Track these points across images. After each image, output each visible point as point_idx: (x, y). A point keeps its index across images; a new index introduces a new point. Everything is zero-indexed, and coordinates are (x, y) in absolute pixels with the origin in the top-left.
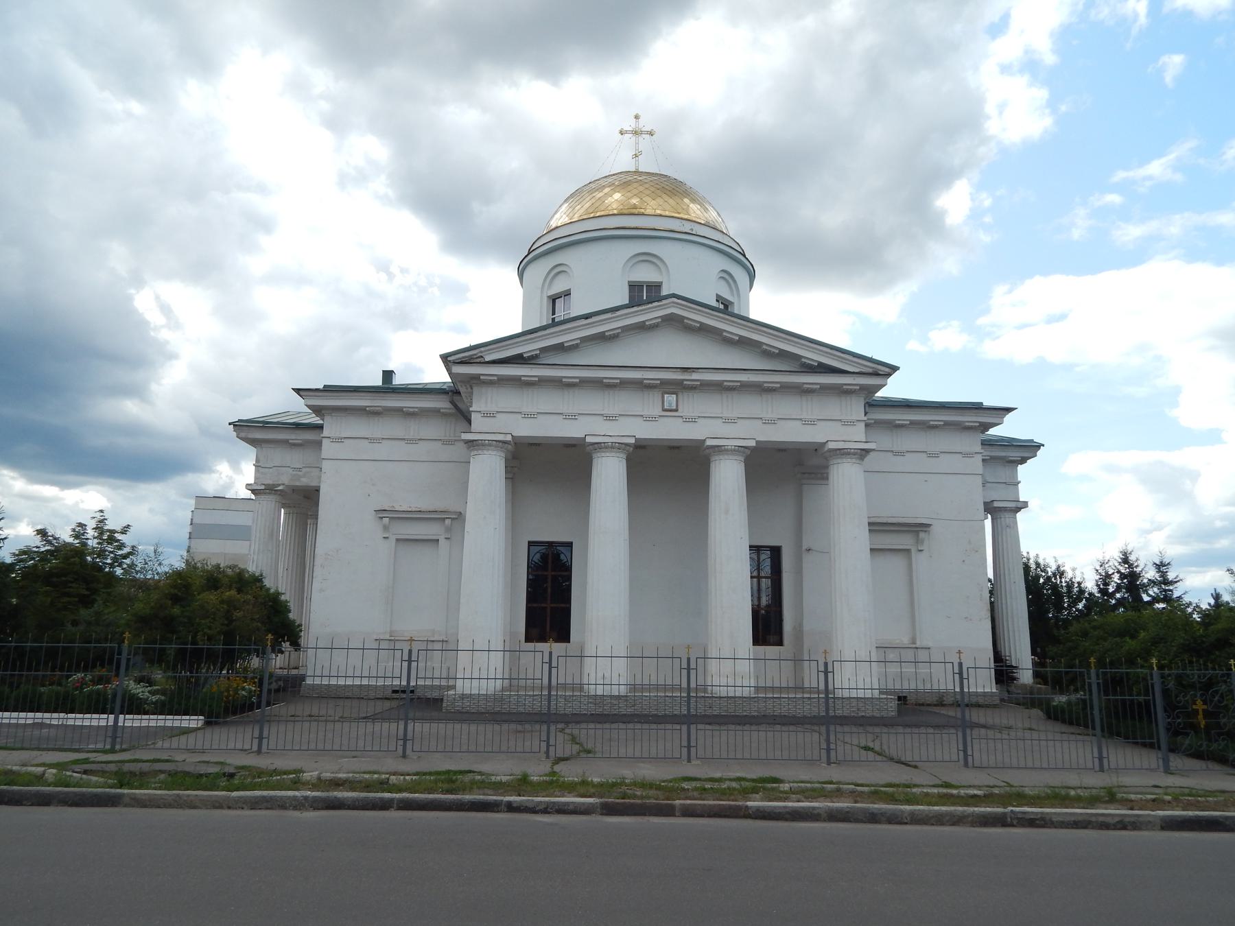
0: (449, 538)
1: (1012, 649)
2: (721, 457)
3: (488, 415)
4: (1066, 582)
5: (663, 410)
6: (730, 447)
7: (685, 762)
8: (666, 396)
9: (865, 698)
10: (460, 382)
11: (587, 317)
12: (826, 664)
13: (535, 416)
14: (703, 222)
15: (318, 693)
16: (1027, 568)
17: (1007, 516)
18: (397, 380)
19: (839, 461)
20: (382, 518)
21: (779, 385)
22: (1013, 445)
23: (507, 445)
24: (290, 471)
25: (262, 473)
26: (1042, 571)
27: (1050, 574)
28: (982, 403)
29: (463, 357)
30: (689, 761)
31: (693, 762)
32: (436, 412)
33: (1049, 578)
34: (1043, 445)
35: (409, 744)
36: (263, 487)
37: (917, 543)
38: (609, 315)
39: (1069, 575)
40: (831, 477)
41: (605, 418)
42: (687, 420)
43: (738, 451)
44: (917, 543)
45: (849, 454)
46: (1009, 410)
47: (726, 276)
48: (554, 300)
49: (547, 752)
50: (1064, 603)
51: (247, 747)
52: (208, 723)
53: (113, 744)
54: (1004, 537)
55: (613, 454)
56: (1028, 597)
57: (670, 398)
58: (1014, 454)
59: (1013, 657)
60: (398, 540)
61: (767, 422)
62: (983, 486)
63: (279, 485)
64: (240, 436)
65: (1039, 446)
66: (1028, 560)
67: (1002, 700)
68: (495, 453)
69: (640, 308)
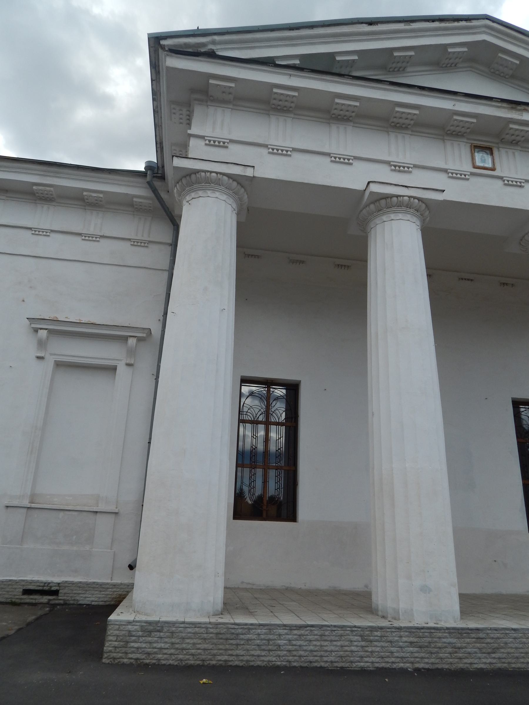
11: (371, 22)
23: (243, 190)
38: (401, 26)
55: (409, 217)
60: (58, 365)
68: (224, 197)
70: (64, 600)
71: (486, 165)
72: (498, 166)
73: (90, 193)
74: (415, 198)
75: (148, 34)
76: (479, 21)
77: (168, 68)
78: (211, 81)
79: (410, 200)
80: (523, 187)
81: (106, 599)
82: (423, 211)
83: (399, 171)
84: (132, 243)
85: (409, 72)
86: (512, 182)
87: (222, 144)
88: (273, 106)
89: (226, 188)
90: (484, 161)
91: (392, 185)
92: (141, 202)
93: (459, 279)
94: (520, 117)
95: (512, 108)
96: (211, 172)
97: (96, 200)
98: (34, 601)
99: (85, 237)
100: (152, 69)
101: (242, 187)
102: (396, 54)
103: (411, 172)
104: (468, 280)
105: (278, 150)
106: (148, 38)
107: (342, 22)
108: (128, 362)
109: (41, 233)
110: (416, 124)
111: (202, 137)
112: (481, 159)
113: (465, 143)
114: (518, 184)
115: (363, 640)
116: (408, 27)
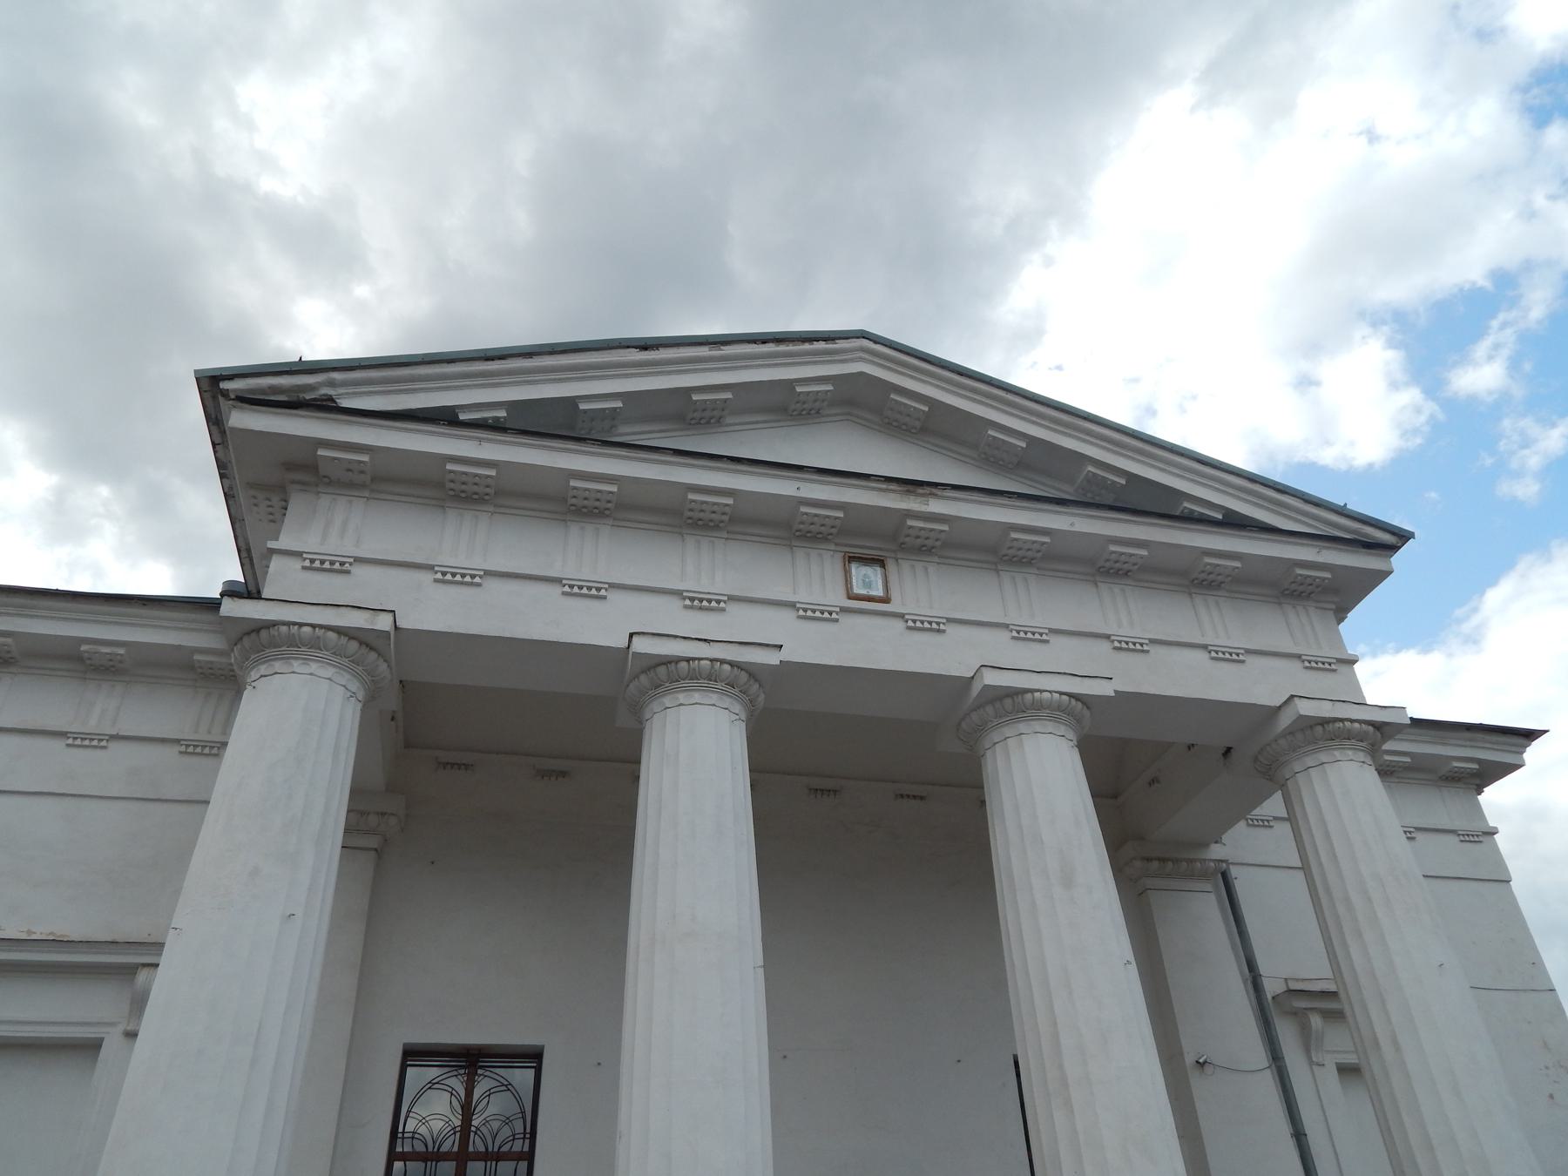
2: (1022, 727)
3: (327, 565)
5: (850, 598)
6: (1046, 695)
10: (251, 485)
11: (645, 345)
19: (1323, 757)
23: (373, 655)
38: (704, 351)
46: (1530, 735)
55: (714, 698)
68: (329, 672)
71: (873, 593)
73: (95, 647)
74: (723, 662)
75: (196, 371)
76: (849, 340)
78: (321, 452)
79: (712, 667)
80: (944, 631)
82: (745, 684)
83: (701, 608)
85: (731, 425)
86: (922, 622)
87: (337, 567)
88: (452, 493)
89: (334, 653)
90: (868, 585)
91: (678, 639)
92: (212, 662)
93: (897, 795)
94: (923, 508)
96: (301, 625)
97: (111, 660)
99: (75, 739)
100: (212, 427)
101: (372, 649)
102: (695, 397)
103: (723, 610)
104: (914, 797)
105: (454, 575)
106: (196, 378)
107: (589, 346)
108: (129, 1028)
110: (732, 520)
111: (298, 554)
112: (867, 579)
113: (832, 553)
114: (934, 626)
116: (716, 353)
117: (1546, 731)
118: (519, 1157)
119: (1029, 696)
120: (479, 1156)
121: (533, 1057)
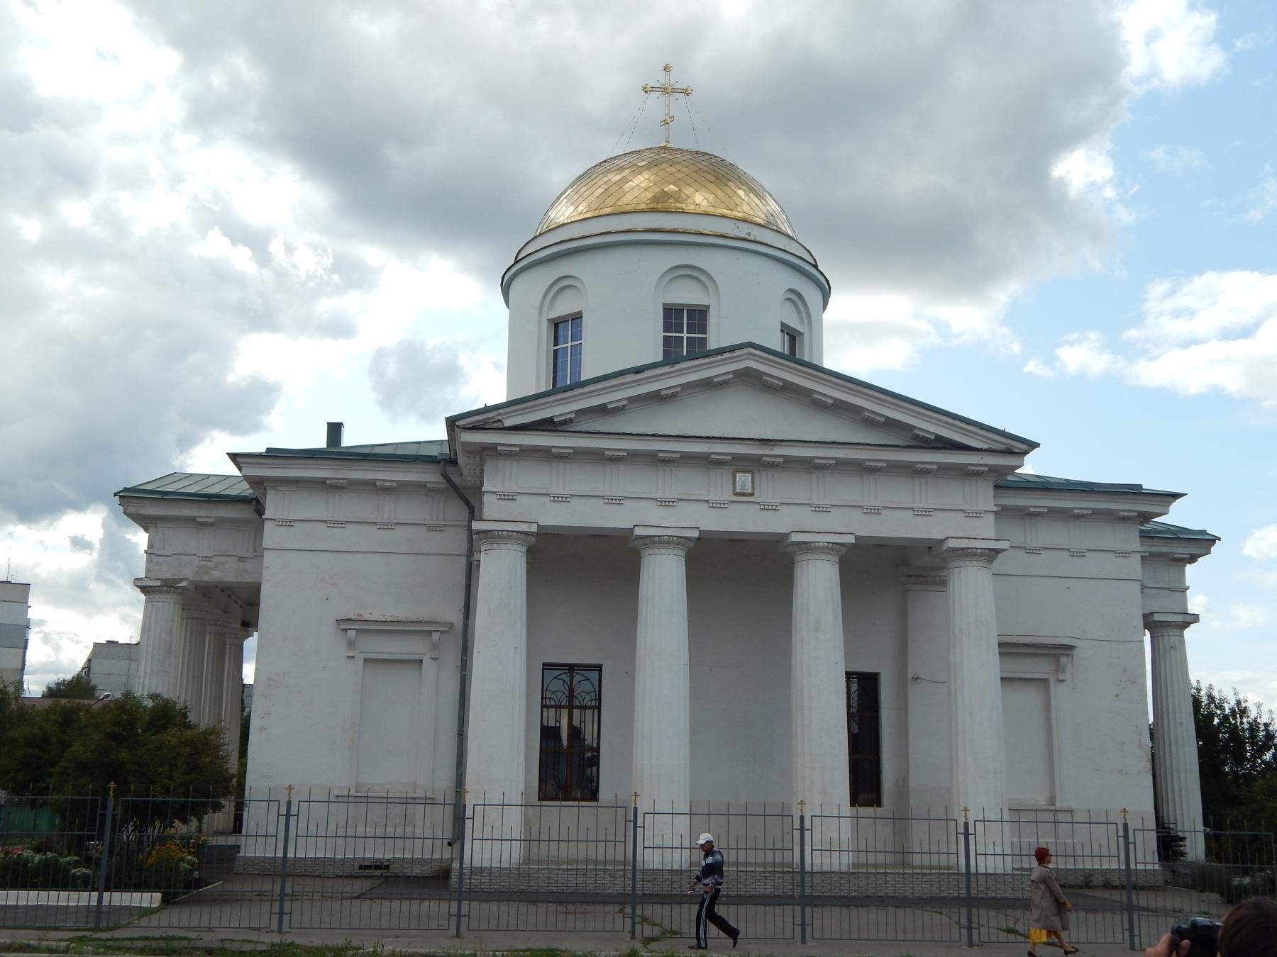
0: (437, 659)
1: (1178, 812)
2: (810, 557)
3: (507, 497)
4: (1248, 723)
7: (799, 944)
8: (738, 475)
9: (995, 874)
11: (638, 370)
12: (966, 824)
13: (568, 499)
14: (762, 222)
15: (257, 869)
16: (1196, 702)
17: (1171, 634)
18: (349, 439)
19: (962, 564)
20: (346, 630)
21: (885, 465)
22: (1179, 538)
24: (196, 560)
25: (157, 563)
26: (1217, 708)
27: (1227, 711)
28: (1140, 486)
29: (477, 422)
30: (804, 941)
31: (809, 944)
32: (421, 487)
33: (1225, 718)
34: (1219, 539)
35: (464, 920)
36: (158, 583)
37: (1057, 671)
39: (1253, 713)
40: (951, 585)
41: (659, 503)
42: (766, 507)
43: (832, 549)
44: (1057, 671)
45: (975, 555)
46: (1175, 496)
47: (795, 298)
48: (557, 324)
49: (633, 932)
50: (1247, 751)
51: (265, 924)
52: (166, 901)
53: (97, 923)
54: (1167, 661)
55: (670, 551)
56: (1198, 743)
57: (743, 479)
58: (1180, 550)
59: (1179, 823)
60: (366, 660)
61: (869, 511)
62: (1142, 592)
63: (181, 580)
64: (128, 511)
65: (1213, 540)
66: (1199, 690)
67: (1166, 882)
68: (514, 547)
69: (707, 360)
70: (395, 873)
72: (757, 492)
77: (463, 443)
81: (429, 872)
84: (428, 528)
95: (764, 444)
98: (369, 874)
109: (336, 525)
115: (611, 877)
117: (1186, 494)
118: (594, 708)
119: (813, 544)
120: (577, 707)
121: (599, 668)
